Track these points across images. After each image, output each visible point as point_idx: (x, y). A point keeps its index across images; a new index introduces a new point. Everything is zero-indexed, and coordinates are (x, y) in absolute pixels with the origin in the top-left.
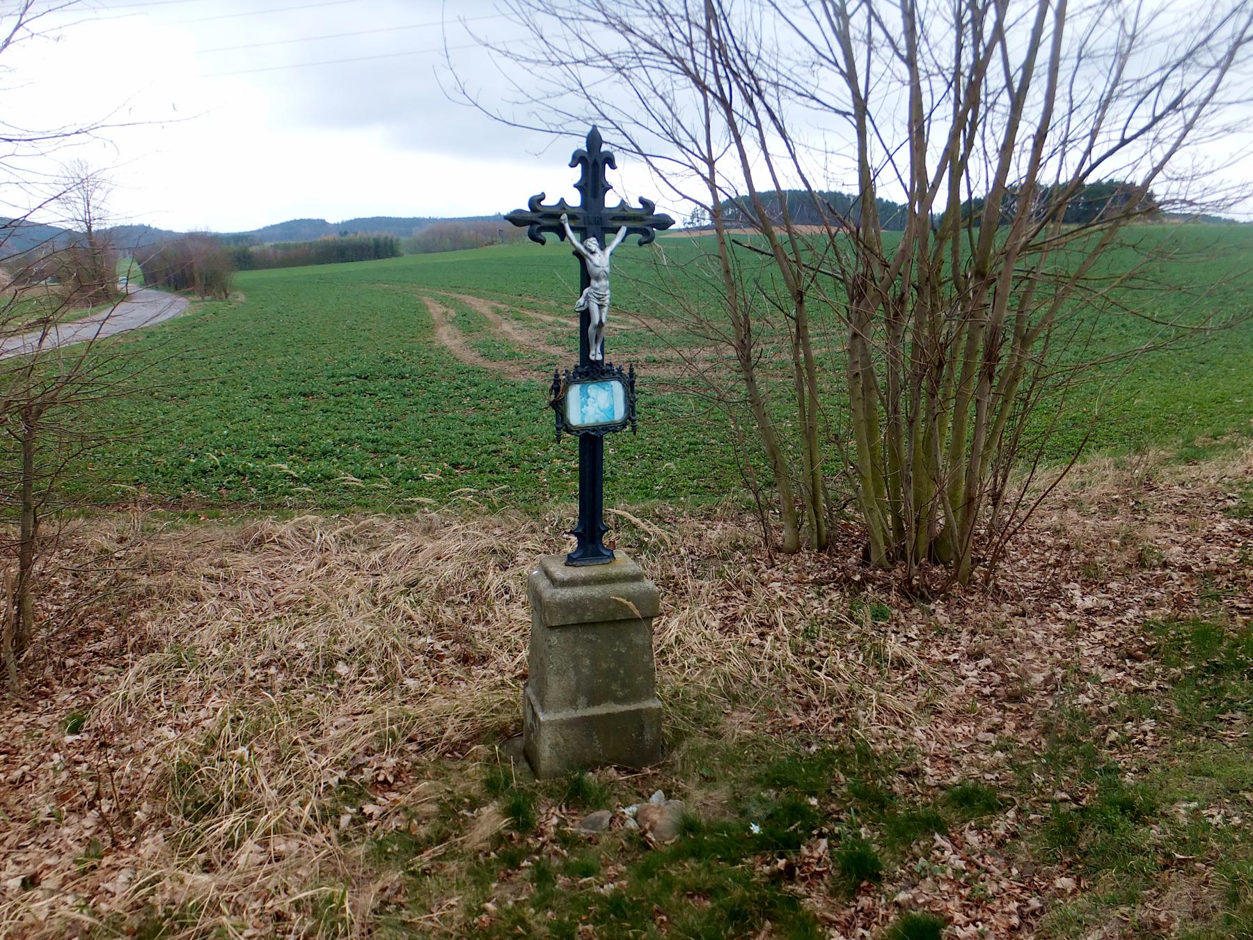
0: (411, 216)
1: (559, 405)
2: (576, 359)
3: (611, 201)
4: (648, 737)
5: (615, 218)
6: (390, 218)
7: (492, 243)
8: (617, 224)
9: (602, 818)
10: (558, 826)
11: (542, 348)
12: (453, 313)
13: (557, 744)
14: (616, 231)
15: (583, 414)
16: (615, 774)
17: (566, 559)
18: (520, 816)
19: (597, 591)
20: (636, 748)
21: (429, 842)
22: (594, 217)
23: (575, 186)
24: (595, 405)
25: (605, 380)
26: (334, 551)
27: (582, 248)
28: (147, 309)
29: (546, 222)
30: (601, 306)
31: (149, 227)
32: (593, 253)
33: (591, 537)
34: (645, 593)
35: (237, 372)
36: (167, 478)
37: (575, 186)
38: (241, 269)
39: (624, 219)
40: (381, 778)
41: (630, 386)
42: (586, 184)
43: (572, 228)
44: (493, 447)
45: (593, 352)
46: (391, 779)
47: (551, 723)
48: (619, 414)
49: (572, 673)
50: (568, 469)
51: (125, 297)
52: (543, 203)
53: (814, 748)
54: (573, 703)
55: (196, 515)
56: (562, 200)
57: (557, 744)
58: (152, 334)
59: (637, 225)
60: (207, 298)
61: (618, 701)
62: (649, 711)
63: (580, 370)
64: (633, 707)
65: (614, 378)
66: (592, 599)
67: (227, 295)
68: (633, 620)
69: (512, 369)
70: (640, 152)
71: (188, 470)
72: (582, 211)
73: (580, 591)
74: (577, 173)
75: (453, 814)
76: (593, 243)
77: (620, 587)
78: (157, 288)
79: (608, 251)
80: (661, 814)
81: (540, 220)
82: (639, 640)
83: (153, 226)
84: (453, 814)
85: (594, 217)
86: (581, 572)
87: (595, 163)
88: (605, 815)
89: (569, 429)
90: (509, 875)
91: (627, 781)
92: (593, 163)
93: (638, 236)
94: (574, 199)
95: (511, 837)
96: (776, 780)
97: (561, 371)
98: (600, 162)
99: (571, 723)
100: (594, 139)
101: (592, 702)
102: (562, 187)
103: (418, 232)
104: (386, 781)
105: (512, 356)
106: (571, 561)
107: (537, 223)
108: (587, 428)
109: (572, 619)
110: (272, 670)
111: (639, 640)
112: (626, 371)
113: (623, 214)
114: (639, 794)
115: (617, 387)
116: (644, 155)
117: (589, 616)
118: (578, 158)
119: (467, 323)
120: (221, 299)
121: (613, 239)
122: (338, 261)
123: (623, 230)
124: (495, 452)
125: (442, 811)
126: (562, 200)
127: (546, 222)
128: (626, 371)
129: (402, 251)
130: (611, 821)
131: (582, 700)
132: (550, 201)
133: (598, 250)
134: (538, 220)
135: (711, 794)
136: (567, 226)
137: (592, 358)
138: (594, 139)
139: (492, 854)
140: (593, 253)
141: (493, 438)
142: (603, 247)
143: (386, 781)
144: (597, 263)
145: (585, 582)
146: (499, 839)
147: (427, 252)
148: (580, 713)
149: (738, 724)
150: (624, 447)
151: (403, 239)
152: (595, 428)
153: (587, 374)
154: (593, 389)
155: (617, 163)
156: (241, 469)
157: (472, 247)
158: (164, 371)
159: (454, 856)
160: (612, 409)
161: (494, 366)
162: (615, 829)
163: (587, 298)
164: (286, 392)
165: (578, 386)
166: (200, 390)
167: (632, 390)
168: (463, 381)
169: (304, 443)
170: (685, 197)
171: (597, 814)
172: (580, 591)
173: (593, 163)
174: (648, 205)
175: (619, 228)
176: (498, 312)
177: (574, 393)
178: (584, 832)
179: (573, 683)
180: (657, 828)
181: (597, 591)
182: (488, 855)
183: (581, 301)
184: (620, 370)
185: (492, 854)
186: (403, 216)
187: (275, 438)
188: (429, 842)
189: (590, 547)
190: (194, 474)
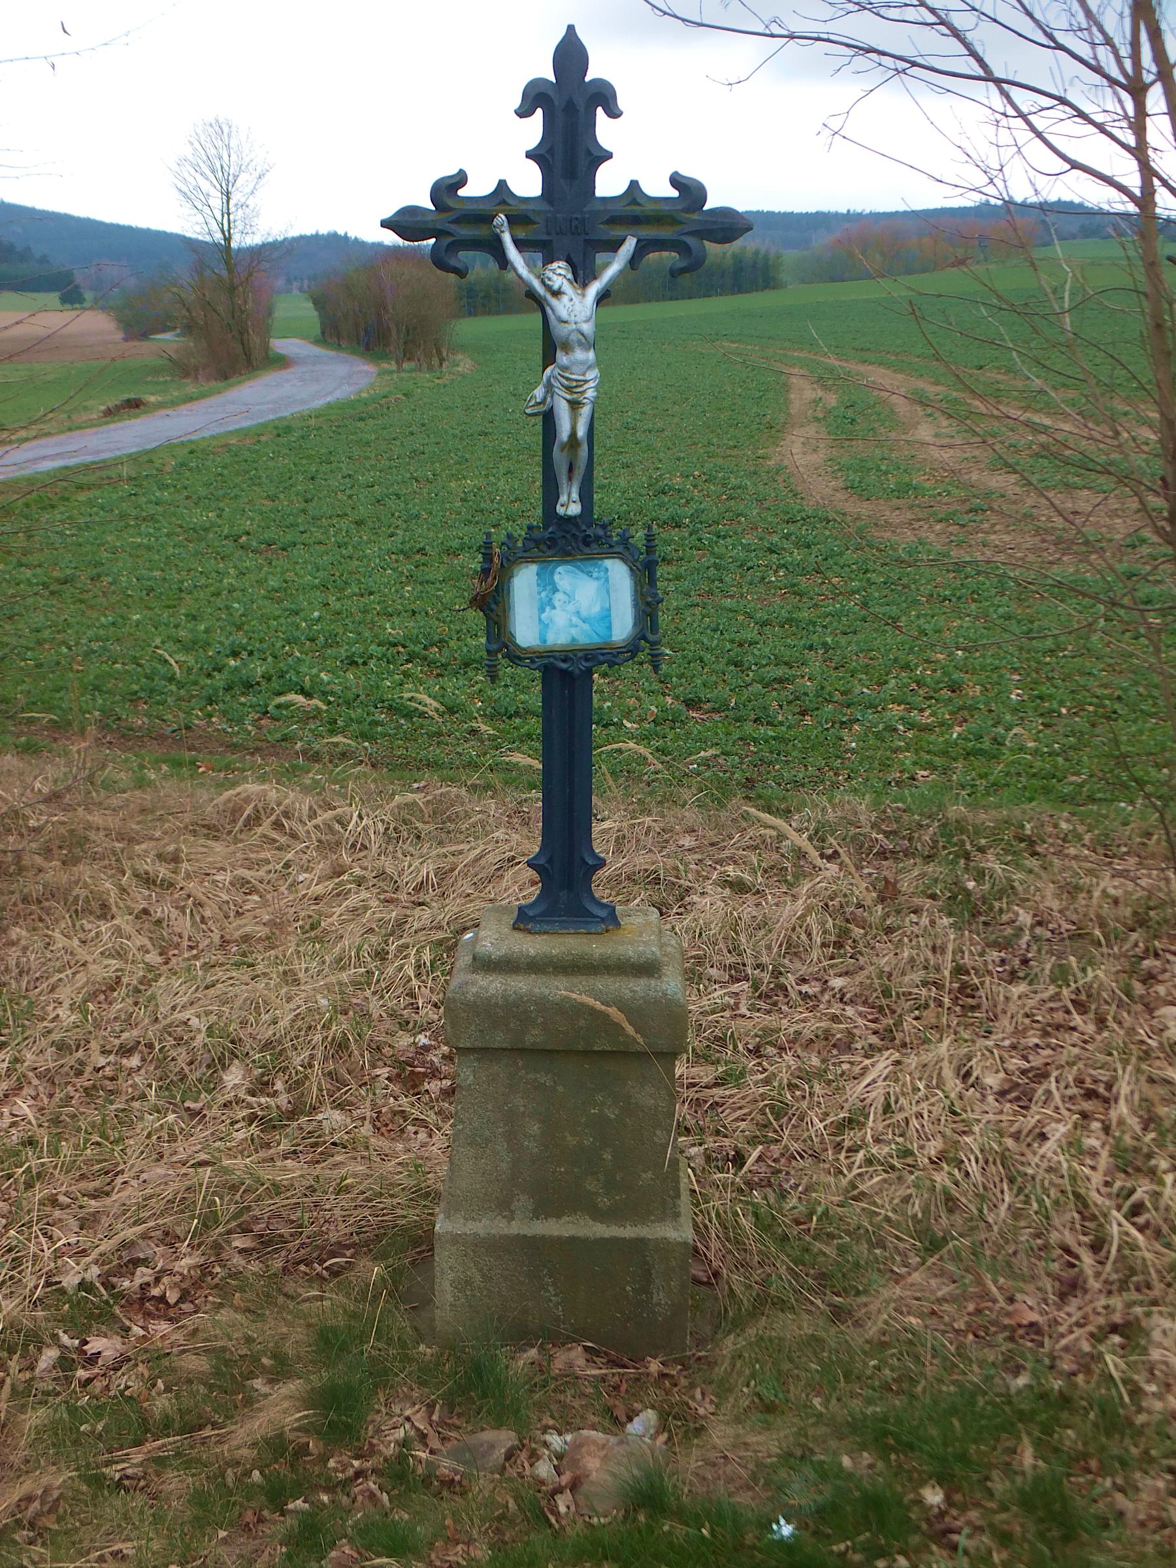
0: (812, 209)
1: (492, 603)
2: (536, 515)
3: (609, 183)
4: (659, 1297)
5: (615, 220)
6: (791, 215)
7: (961, 262)
8: (616, 232)
9: (492, 1447)
10: (405, 1443)
11: (975, 476)
12: (832, 400)
13: (469, 1282)
14: (614, 246)
15: (544, 626)
16: (581, 1362)
17: (510, 919)
18: (339, 1415)
19: (559, 988)
20: (636, 1320)
21: (166, 1427)
22: (569, 211)
23: (530, 155)
24: (571, 606)
25: (591, 558)
26: (374, 848)
27: (536, 284)
28: (312, 380)
29: (465, 232)
30: (575, 405)
31: (346, 238)
32: (557, 293)
33: (566, 879)
34: (657, 1002)
35: (391, 503)
36: (182, 692)
37: (530, 155)
38: (471, 314)
39: (635, 221)
40: (156, 1292)
41: (645, 573)
42: (551, 151)
43: (518, 243)
44: (780, 672)
45: (563, 498)
46: (172, 1297)
47: (455, 1239)
48: (622, 627)
49: (502, 1146)
50: (911, 726)
51: (283, 362)
52: (462, 192)
53: (1022, 1381)
54: (504, 1206)
55: (193, 763)
56: (502, 184)
57: (469, 1282)
58: (288, 430)
59: (666, 233)
60: (406, 365)
61: (599, 1215)
62: (664, 1247)
63: (536, 534)
64: (628, 1232)
65: (611, 554)
66: (543, 1004)
67: (442, 360)
68: (626, 1055)
69: (895, 518)
70: (989, 77)
71: (219, 680)
72: (545, 207)
73: (521, 985)
74: (533, 129)
75: (231, 1382)
76: (559, 274)
77: (602, 983)
78: (339, 347)
79: (594, 289)
80: (605, 1459)
81: (452, 228)
82: (647, 1097)
83: (352, 235)
84: (231, 1382)
85: (569, 211)
86: (531, 946)
87: (570, 108)
88: (505, 1438)
89: (516, 656)
90: (261, 1520)
91: (603, 1379)
92: (569, 104)
93: (669, 257)
94: (528, 182)
95: (303, 1450)
96: (880, 1437)
97: (499, 536)
98: (580, 102)
99: (497, 1246)
100: (570, 54)
101: (545, 1208)
102: (504, 158)
103: (821, 240)
104: (162, 1299)
105: (903, 490)
106: (524, 920)
107: (449, 234)
108: (550, 653)
109: (499, 1039)
110: (135, 1061)
111: (647, 1097)
112: (639, 536)
113: (634, 208)
114: (609, 1411)
115: (618, 573)
116: (998, 82)
117: (535, 1037)
118: (535, 98)
119: (850, 421)
120: (430, 368)
121: (607, 265)
122: (664, 298)
123: (630, 244)
124: (780, 681)
125: (218, 1373)
126: (502, 184)
127: (465, 232)
128: (639, 536)
129: (784, 277)
130: (509, 1455)
131: (523, 1202)
132: (478, 187)
133: (567, 287)
134: (452, 223)
135: (752, 1439)
136: (507, 238)
137: (560, 510)
138: (570, 54)
139: (256, 1473)
140: (557, 293)
141: (787, 654)
142: (581, 278)
143: (162, 1299)
144: (564, 314)
145: (535, 966)
146: (275, 1446)
147: (833, 280)
148: (516, 1228)
149: (904, 1299)
150: (1044, 689)
151: (790, 256)
152: (568, 654)
153: (552, 543)
154: (564, 576)
155: (621, 103)
156: (307, 683)
157: (924, 271)
158: (273, 498)
159: (189, 1463)
160: (606, 617)
161: (864, 509)
162: (512, 1472)
163: (549, 388)
164: (455, 544)
165: (533, 568)
166: (319, 536)
167: (652, 581)
168: (787, 537)
169: (441, 643)
170: (1075, 165)
171: (488, 1435)
172: (521, 985)
173: (569, 104)
174: (690, 191)
175: (621, 242)
176: (921, 400)
177: (524, 582)
178: (446, 1466)
179: (504, 1165)
180: (585, 1487)
181: (559, 988)
182: (248, 1474)
183: (539, 392)
184: (625, 540)
185: (256, 1473)
186: (797, 209)
187: (390, 630)
188: (166, 1427)
189: (563, 895)
190: (229, 688)
